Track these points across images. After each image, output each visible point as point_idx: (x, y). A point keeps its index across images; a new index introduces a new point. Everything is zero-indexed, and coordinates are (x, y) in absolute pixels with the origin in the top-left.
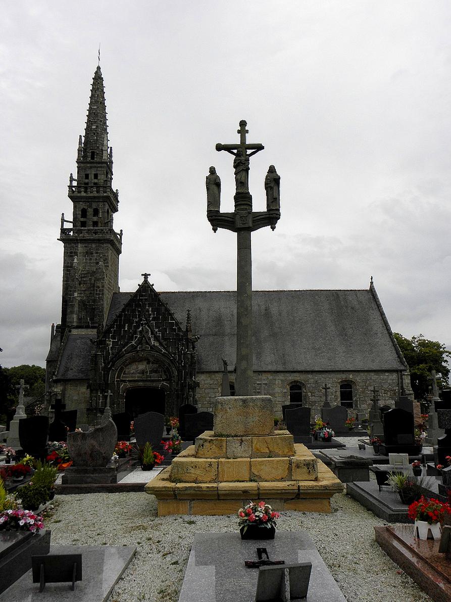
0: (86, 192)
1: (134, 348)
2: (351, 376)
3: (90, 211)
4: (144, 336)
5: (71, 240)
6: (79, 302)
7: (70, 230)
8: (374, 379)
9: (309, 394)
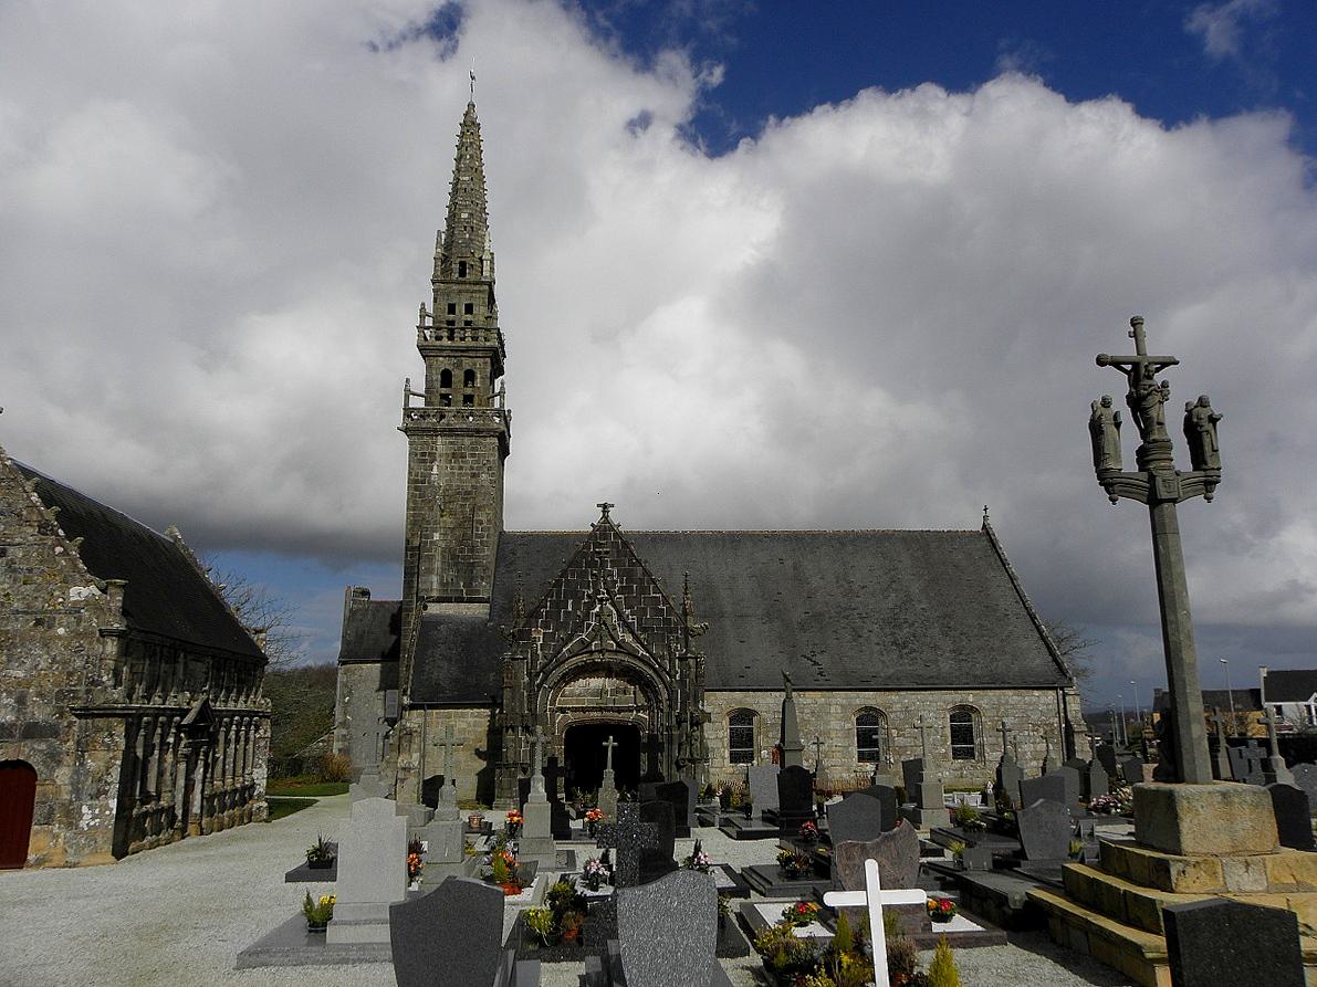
0: (451, 338)
1: (585, 645)
3: (458, 376)
6: (443, 551)
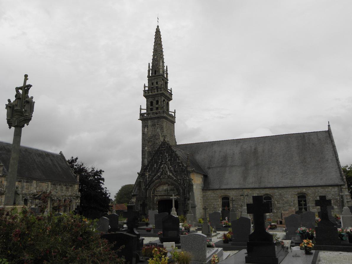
0: (151, 92)
1: (159, 177)
2: (304, 190)
3: (155, 102)
4: (163, 170)
5: (145, 119)
6: (148, 152)
7: (145, 113)
8: (321, 191)
9: (276, 202)
